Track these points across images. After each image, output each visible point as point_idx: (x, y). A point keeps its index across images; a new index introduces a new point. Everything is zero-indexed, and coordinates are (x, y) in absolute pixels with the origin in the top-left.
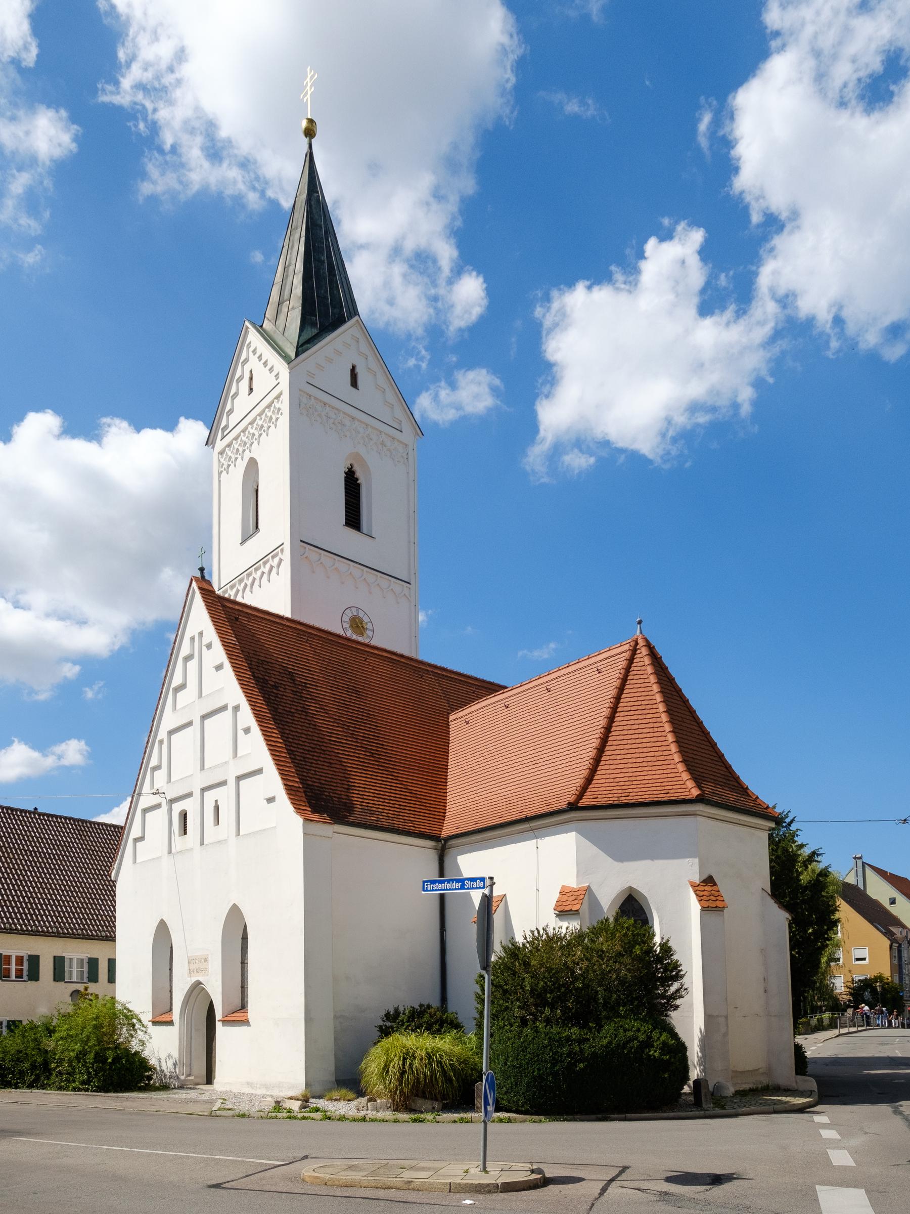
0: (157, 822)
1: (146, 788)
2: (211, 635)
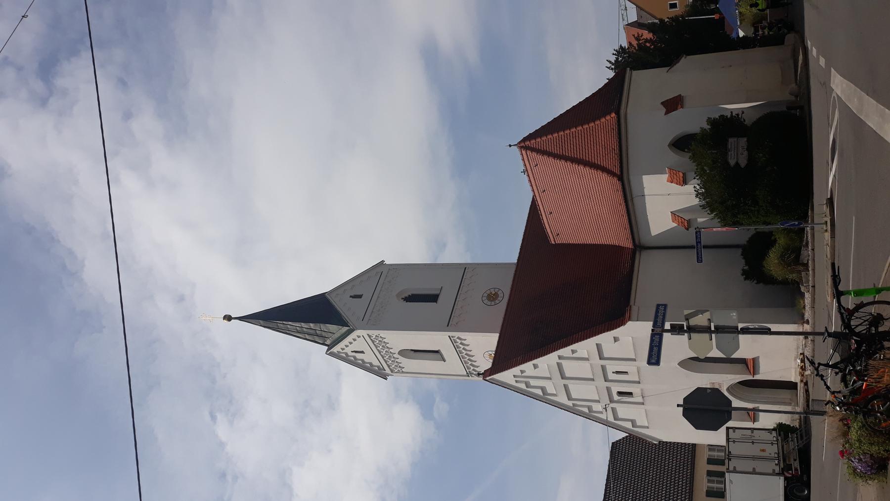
0: (624, 411)
1: (603, 416)
2: (516, 370)
